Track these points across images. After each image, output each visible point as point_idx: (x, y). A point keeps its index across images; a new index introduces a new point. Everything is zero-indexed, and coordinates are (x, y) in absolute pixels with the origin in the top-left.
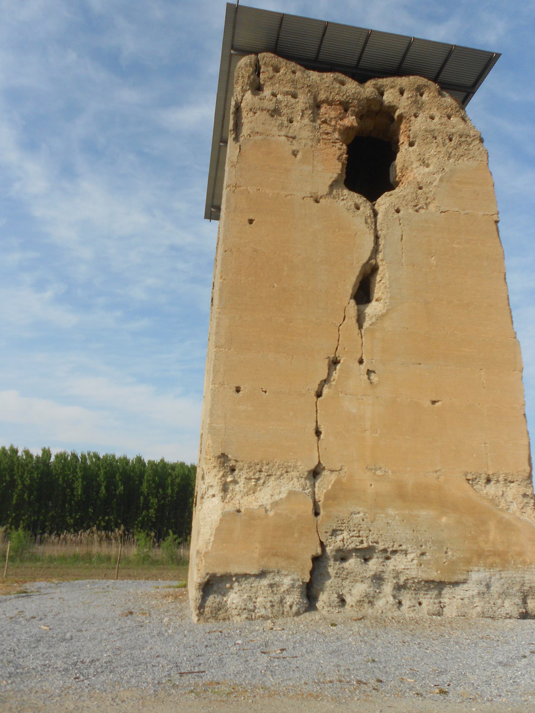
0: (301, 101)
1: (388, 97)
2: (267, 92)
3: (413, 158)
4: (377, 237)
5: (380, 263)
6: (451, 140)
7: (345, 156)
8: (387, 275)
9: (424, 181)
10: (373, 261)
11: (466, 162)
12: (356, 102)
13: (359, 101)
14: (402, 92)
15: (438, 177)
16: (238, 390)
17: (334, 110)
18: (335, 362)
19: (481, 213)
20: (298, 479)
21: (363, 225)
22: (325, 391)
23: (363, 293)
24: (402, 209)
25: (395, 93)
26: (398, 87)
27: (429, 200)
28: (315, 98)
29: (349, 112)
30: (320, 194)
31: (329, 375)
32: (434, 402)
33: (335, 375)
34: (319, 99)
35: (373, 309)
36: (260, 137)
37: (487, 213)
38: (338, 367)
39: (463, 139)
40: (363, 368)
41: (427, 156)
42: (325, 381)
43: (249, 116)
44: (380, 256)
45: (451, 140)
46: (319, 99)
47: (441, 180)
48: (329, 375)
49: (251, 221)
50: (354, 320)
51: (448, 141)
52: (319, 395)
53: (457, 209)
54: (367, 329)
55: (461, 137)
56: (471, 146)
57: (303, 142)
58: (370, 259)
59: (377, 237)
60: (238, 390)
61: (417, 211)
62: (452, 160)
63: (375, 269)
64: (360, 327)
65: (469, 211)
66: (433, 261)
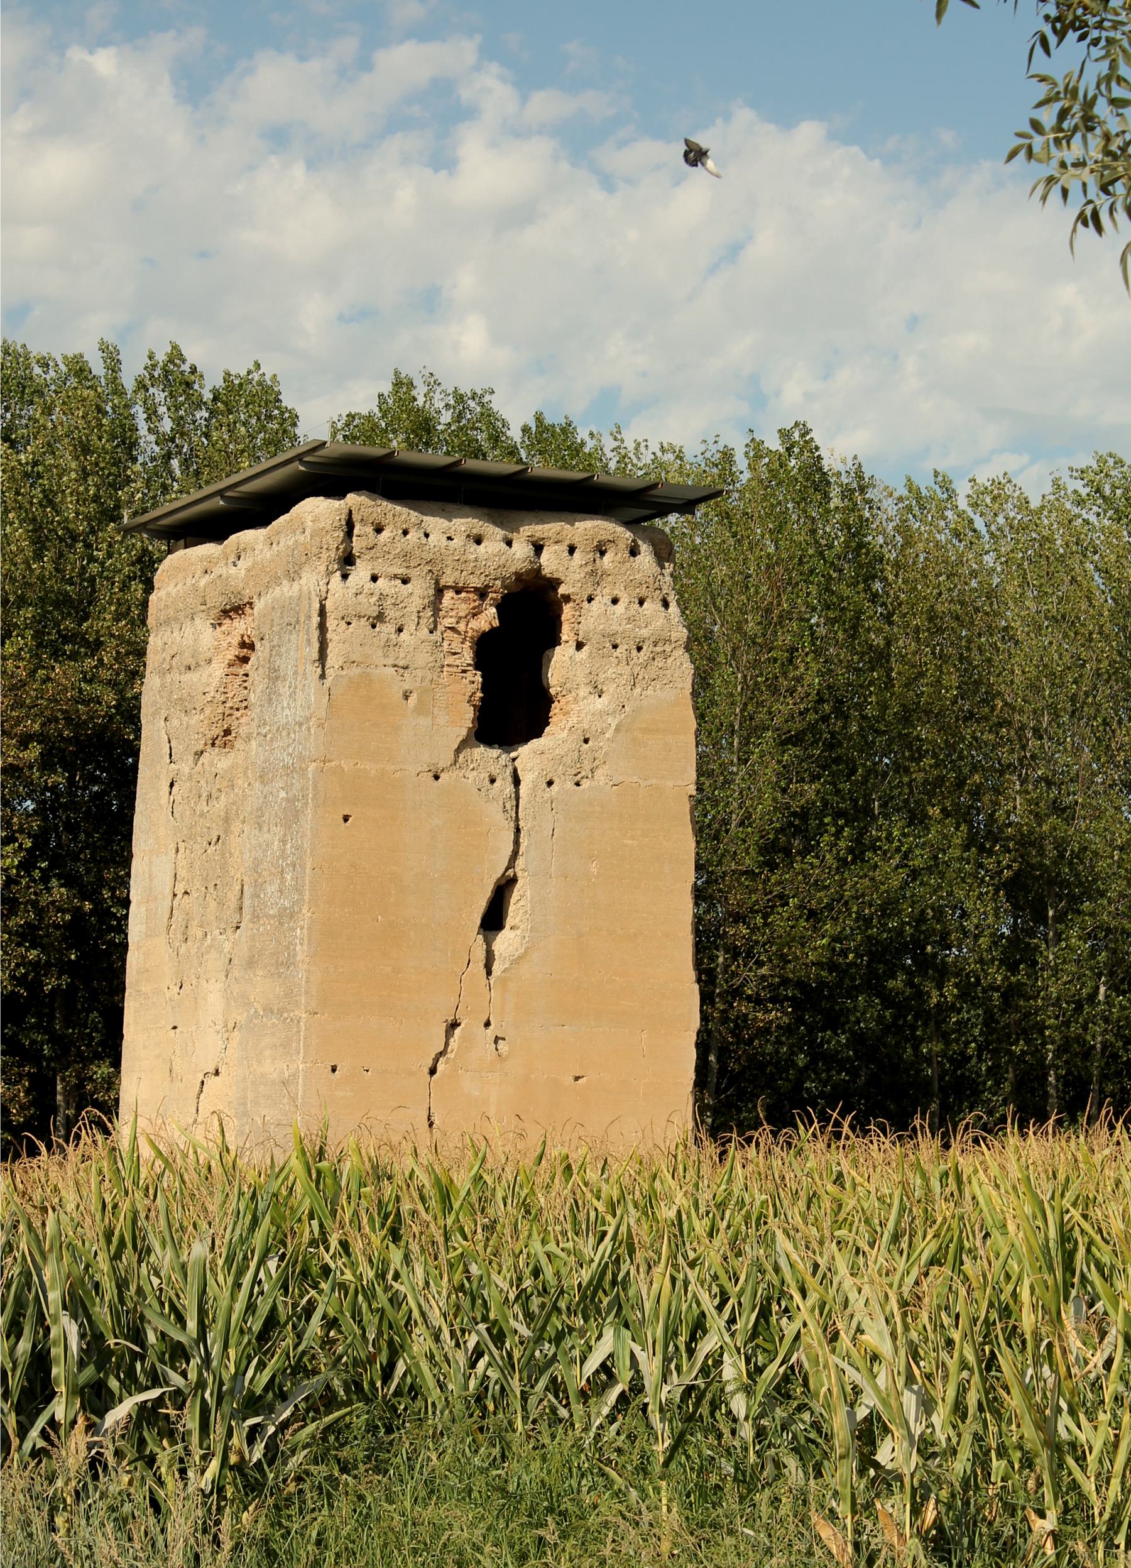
0: (418, 592)
1: (551, 562)
2: (360, 573)
3: (581, 676)
4: (518, 830)
5: (519, 874)
6: (639, 649)
7: (479, 694)
8: (528, 893)
9: (594, 728)
10: (510, 872)
11: (659, 692)
12: (498, 583)
13: (504, 579)
14: (572, 550)
15: (613, 722)
16: (334, 1070)
17: (465, 600)
18: (454, 1025)
19: (670, 784)
20: (971, 686)
21: (500, 816)
22: (440, 1067)
23: (493, 919)
24: (556, 781)
25: (564, 548)
26: (567, 542)
27: (597, 762)
28: (437, 582)
29: (488, 601)
30: (441, 766)
31: (447, 1044)
32: (577, 1078)
33: (454, 1043)
34: (442, 583)
35: (505, 942)
36: (359, 670)
37: (680, 783)
38: (458, 1031)
39: (658, 649)
40: (491, 1032)
41: (602, 676)
42: (441, 1054)
43: (340, 630)
44: (520, 862)
45: (639, 649)
46: (442, 583)
47: (617, 730)
48: (447, 1044)
49: (346, 819)
50: (482, 964)
51: (634, 652)
52: (433, 1071)
53: (636, 779)
54: (498, 978)
55: (655, 644)
56: (669, 661)
57: (419, 673)
58: (507, 869)
59: (518, 830)
60: (334, 1070)
61: (578, 784)
62: (638, 690)
63: (513, 881)
64: (489, 973)
65: (654, 781)
66: (594, 868)
